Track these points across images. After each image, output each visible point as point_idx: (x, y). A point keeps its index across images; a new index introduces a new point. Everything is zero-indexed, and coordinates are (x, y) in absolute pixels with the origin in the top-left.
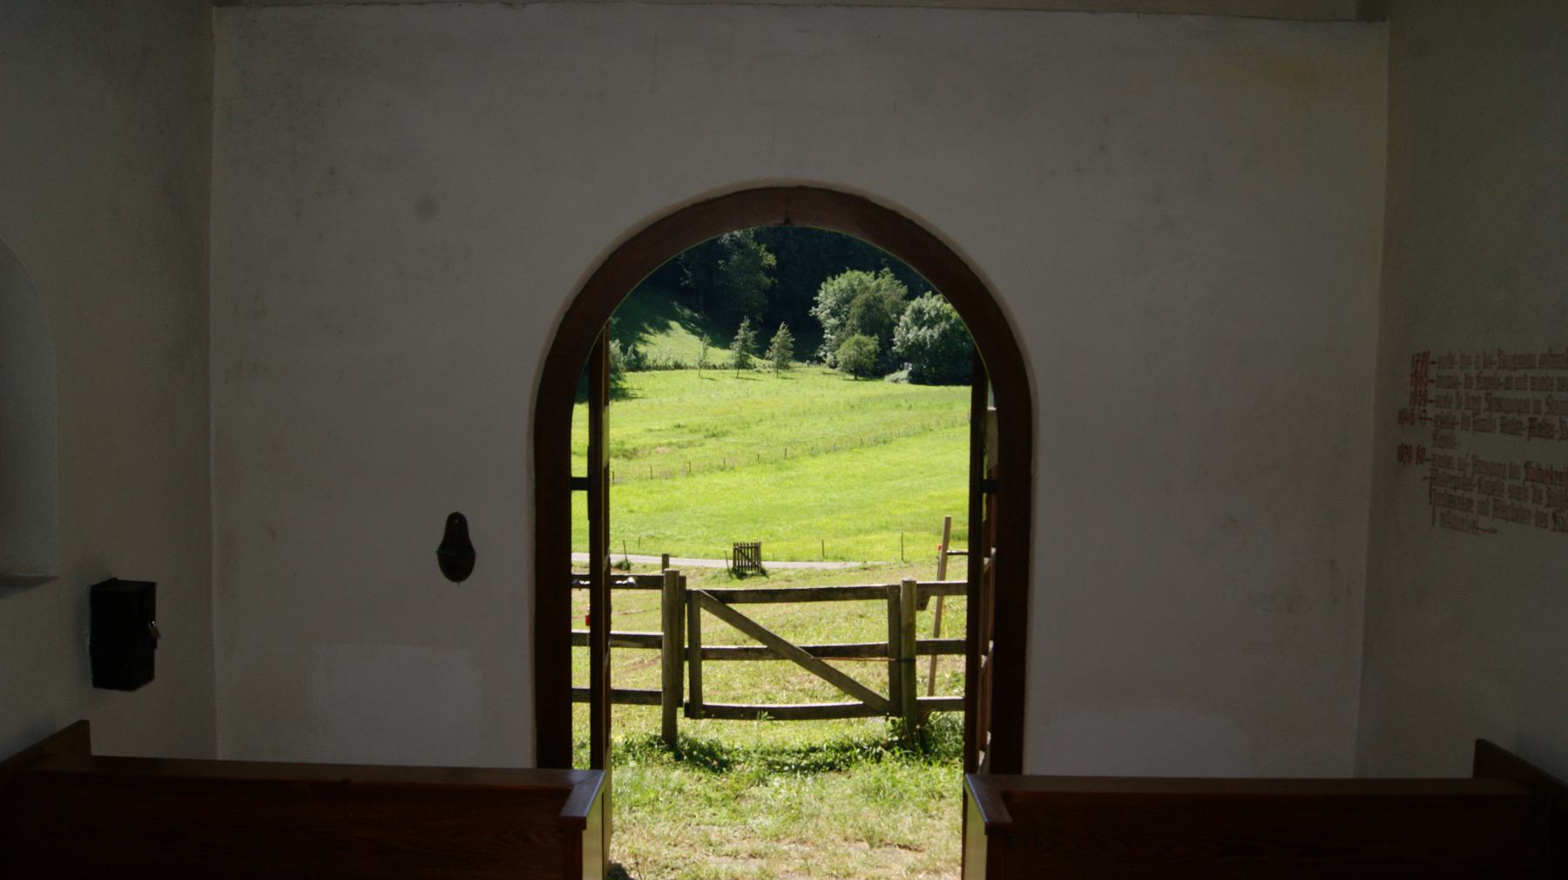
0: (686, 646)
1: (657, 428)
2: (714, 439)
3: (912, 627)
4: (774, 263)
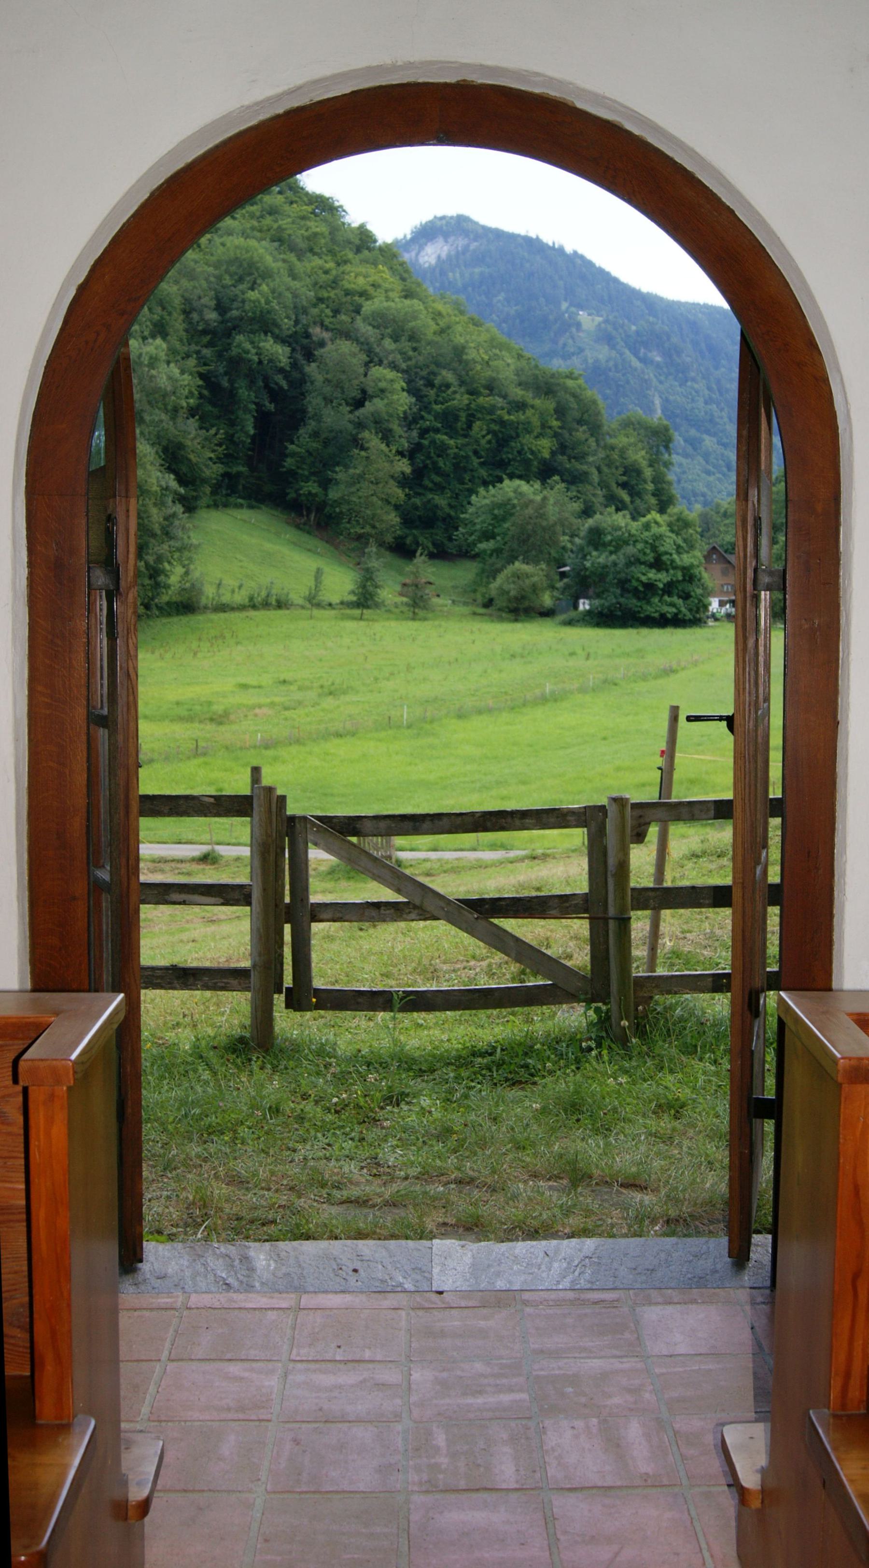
0: (287, 900)
1: (254, 683)
2: (331, 697)
3: (623, 867)
4: (408, 470)
